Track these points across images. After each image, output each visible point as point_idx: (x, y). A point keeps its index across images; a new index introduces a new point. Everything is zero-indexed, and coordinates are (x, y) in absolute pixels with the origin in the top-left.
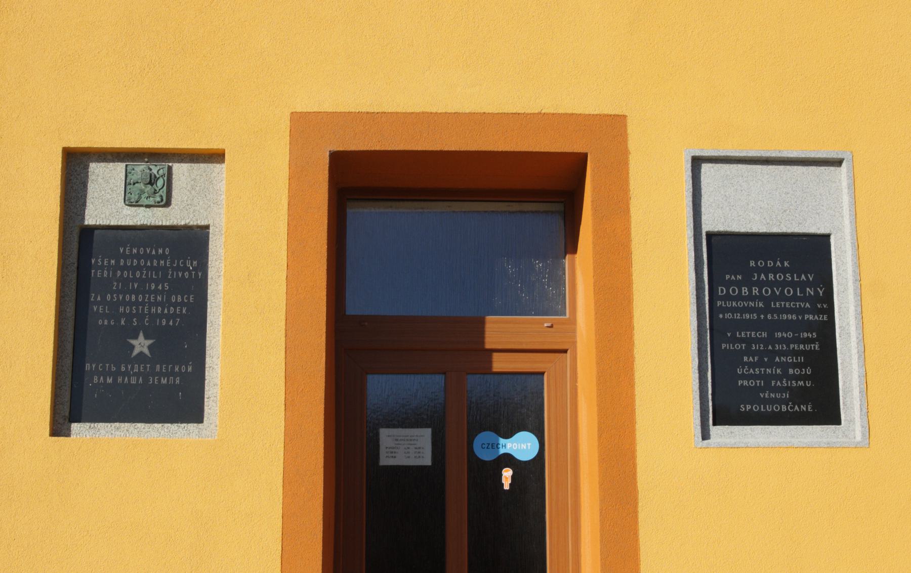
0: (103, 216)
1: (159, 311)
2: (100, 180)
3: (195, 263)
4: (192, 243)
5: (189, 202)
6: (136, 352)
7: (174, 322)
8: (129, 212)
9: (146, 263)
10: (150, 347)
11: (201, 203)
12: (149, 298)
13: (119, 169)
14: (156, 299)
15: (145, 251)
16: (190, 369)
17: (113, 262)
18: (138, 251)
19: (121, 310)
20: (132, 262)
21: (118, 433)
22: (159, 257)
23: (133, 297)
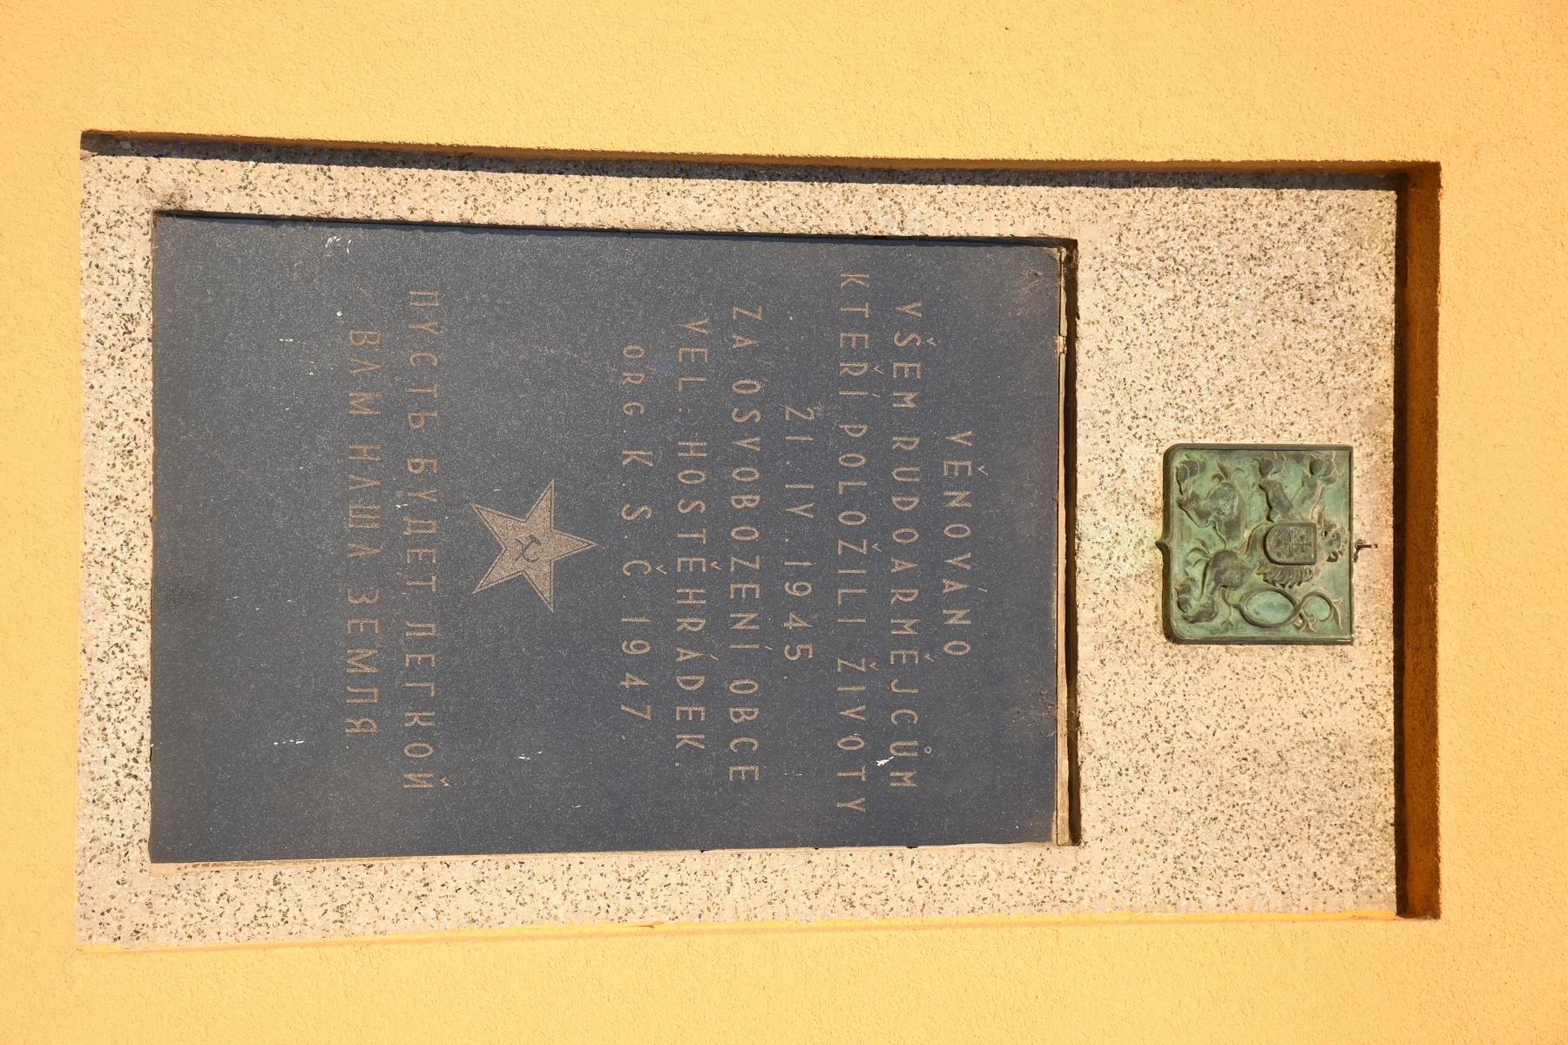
0: (1117, 351)
1: (684, 623)
2: (1274, 333)
3: (907, 779)
4: (992, 771)
5: (1181, 744)
6: (499, 524)
7: (636, 696)
8: (1133, 470)
9: (903, 552)
10: (519, 584)
11: (1178, 800)
12: (744, 575)
13: (1347, 412)
14: (738, 605)
15: (958, 547)
16: (418, 780)
17: (909, 400)
18: (955, 515)
19: (692, 448)
20: (906, 489)
21: (104, 457)
22: (930, 608)
23: (749, 501)
